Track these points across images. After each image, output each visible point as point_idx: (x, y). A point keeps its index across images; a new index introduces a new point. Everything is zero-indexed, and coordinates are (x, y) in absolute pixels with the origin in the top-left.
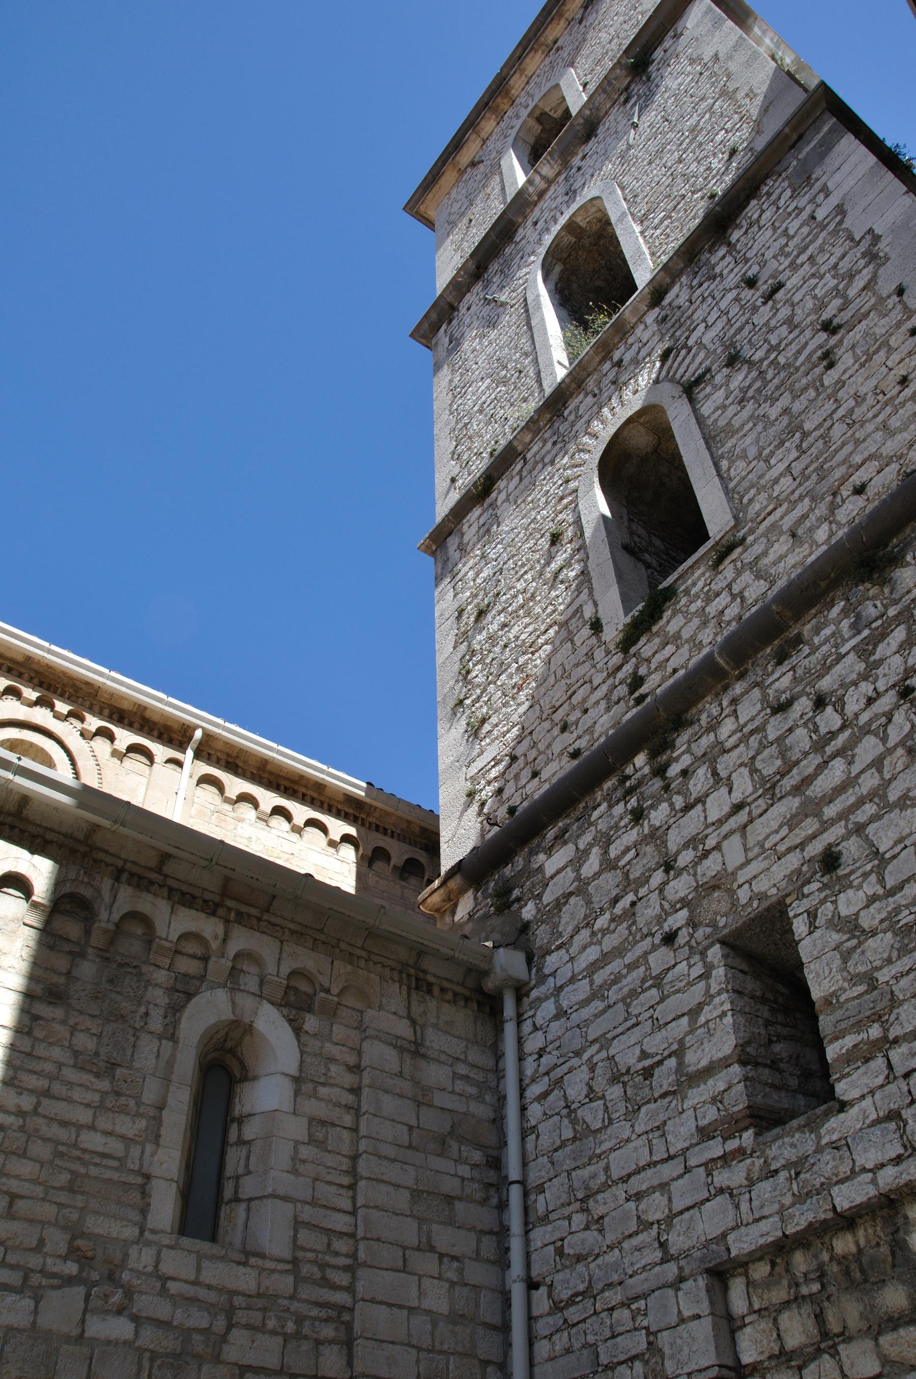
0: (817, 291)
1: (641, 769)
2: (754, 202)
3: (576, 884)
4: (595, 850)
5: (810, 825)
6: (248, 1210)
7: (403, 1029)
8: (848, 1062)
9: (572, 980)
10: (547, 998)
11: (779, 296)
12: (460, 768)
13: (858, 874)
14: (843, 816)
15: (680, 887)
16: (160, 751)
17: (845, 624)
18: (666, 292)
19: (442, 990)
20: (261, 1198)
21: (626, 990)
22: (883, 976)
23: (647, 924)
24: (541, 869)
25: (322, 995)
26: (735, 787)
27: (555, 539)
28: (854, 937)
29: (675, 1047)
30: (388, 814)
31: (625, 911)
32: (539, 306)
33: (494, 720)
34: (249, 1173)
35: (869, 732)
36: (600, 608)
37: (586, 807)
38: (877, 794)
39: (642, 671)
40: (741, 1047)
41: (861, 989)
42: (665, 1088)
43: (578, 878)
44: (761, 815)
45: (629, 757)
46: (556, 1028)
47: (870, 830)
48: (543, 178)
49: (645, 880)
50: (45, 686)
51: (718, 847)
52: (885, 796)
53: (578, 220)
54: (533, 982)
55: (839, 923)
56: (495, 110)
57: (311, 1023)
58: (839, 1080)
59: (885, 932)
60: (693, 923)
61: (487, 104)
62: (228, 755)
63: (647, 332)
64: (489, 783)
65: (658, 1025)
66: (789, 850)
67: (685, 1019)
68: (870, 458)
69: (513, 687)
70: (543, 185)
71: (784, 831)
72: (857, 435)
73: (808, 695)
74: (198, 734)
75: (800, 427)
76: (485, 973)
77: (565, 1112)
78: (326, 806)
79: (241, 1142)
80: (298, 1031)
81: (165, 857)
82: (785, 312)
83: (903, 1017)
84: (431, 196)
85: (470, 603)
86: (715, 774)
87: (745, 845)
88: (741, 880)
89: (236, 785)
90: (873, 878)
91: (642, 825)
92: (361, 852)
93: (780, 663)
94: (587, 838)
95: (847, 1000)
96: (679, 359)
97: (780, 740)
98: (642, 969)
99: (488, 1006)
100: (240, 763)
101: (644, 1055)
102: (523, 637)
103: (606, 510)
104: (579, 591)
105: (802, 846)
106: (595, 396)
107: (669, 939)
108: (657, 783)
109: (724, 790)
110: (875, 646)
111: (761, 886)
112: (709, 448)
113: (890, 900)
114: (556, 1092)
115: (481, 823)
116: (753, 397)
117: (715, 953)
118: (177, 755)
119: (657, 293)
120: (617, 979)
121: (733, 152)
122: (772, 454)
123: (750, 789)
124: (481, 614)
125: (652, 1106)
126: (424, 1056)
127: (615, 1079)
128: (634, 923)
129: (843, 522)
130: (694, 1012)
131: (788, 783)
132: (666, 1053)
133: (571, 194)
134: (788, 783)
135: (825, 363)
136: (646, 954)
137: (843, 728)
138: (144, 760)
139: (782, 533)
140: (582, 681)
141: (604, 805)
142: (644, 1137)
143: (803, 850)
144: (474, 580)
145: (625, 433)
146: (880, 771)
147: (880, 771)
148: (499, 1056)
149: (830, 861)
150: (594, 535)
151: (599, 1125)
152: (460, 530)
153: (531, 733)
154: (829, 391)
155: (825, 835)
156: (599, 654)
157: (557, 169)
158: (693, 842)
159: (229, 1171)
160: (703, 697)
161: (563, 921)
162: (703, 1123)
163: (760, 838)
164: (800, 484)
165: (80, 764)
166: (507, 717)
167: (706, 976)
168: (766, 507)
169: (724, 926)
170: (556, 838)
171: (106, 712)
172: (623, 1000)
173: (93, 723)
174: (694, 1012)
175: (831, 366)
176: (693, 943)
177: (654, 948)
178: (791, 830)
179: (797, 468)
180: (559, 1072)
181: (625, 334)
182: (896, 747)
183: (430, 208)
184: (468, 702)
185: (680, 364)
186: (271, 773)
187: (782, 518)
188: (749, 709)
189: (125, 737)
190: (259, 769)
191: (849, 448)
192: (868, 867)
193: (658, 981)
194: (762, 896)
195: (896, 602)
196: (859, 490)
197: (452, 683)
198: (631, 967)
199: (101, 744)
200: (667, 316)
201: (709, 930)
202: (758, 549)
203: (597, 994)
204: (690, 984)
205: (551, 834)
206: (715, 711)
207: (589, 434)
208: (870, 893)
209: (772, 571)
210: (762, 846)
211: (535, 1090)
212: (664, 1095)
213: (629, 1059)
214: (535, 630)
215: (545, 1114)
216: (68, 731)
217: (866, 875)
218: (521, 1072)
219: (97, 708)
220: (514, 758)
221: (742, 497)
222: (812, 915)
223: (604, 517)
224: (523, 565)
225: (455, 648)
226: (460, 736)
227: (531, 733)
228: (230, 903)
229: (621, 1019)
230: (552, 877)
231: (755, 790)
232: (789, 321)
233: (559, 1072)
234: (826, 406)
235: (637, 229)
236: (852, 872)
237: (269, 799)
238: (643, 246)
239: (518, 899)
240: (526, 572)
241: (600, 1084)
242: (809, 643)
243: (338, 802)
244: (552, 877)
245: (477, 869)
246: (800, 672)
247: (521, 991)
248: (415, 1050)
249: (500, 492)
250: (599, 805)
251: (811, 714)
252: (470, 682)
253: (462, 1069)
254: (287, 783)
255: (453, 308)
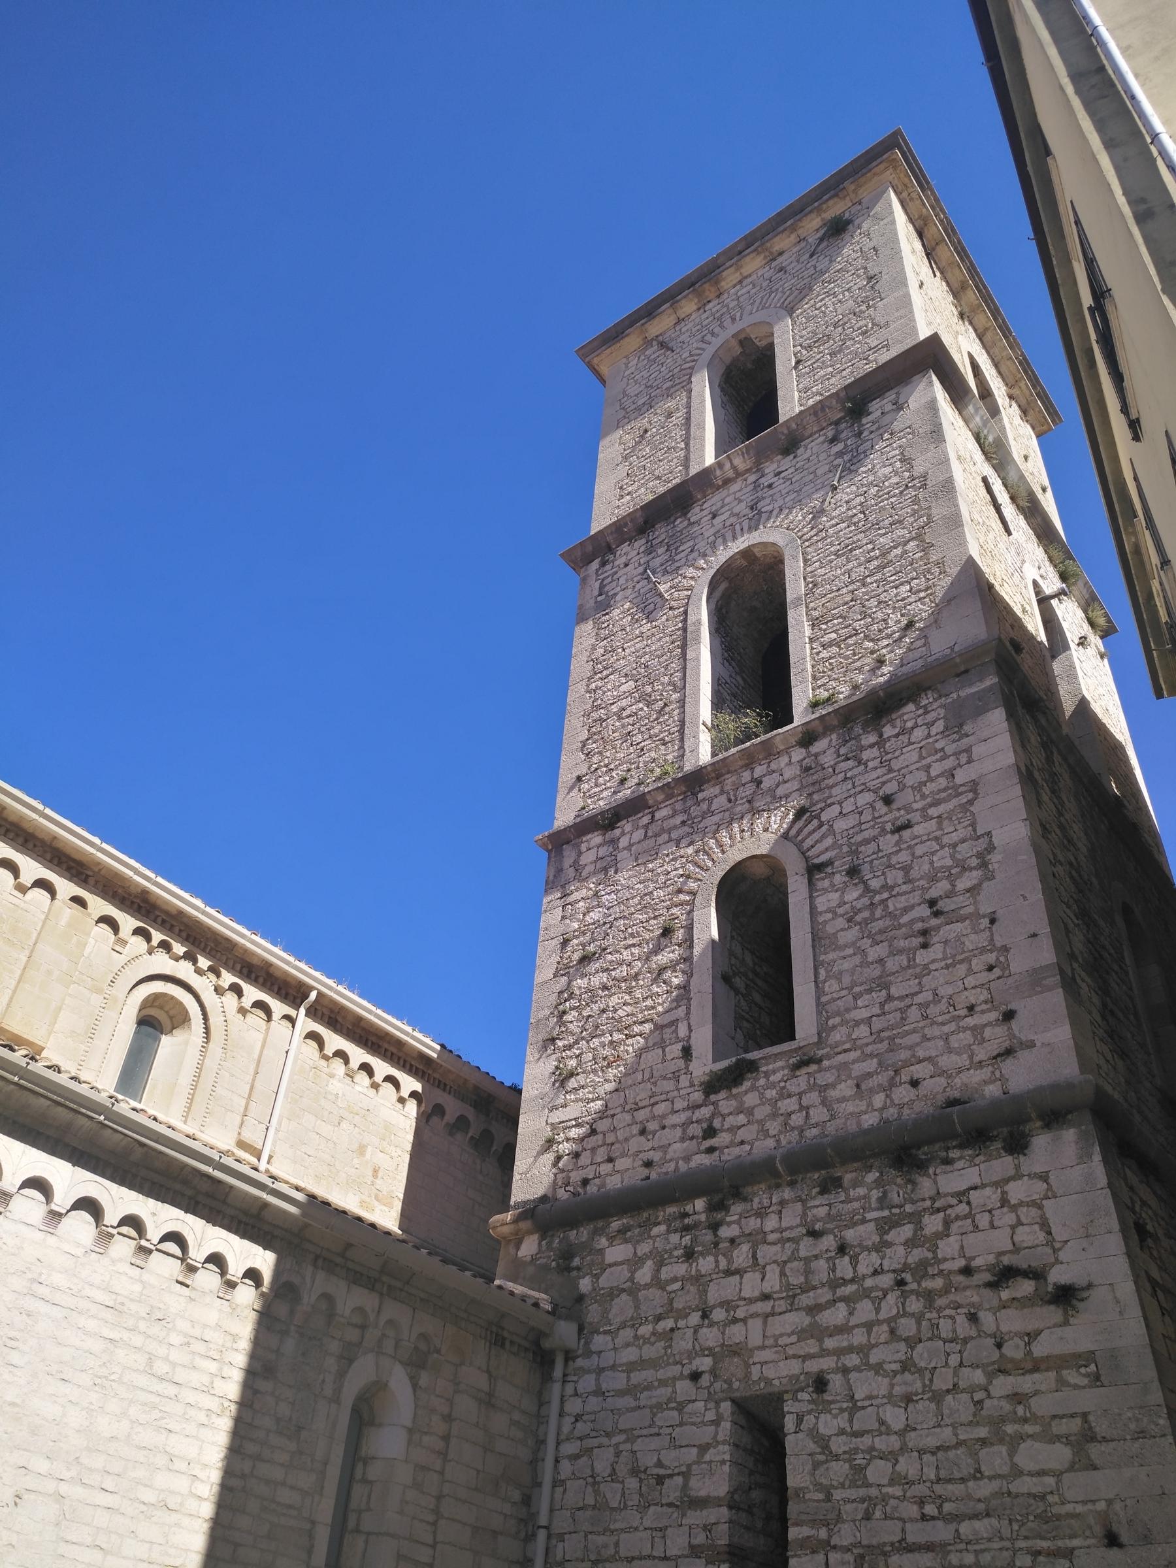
0: (935, 858)
1: (699, 1213)
2: (911, 707)
3: (629, 1284)
4: (649, 1263)
5: (811, 1347)
6: (366, 1542)
7: (483, 1382)
8: (802, 1547)
9: (613, 1367)
10: (589, 1372)
11: (906, 834)
12: (543, 1108)
13: (837, 1406)
14: (839, 1352)
15: (711, 1337)
16: (278, 1008)
17: (875, 1194)
18: (815, 740)
19: (512, 1342)
20: (378, 1534)
21: (654, 1401)
22: (837, 1495)
23: (680, 1353)
24: (601, 1251)
25: (435, 1355)
26: (767, 1278)
27: (667, 932)
28: (823, 1453)
29: (684, 1469)
30: (450, 1071)
31: (664, 1332)
32: (698, 641)
33: (581, 1079)
34: (369, 1509)
35: (868, 1297)
36: (693, 1034)
37: (648, 1219)
38: (863, 1350)
39: (717, 1124)
40: (731, 1493)
41: (821, 1496)
42: (671, 1499)
43: (631, 1279)
44: (780, 1314)
45: (692, 1195)
46: (594, 1403)
47: (853, 1376)
48: (734, 467)
49: (683, 1314)
50: (191, 940)
51: (744, 1321)
52: (867, 1356)
53: (756, 550)
54: (580, 1352)
55: (814, 1434)
56: (699, 295)
57: (424, 1379)
58: (793, 1556)
59: (845, 1461)
60: (713, 1372)
61: (693, 284)
62: (332, 1011)
63: (789, 764)
64: (568, 1140)
65: (674, 1444)
66: (795, 1356)
67: (695, 1451)
68: (929, 1059)
69: (604, 1059)
70: (731, 474)
71: (794, 1338)
72: (926, 1031)
73: (836, 1236)
74: (313, 995)
75: (887, 987)
76: (546, 1335)
77: (590, 1480)
78: (402, 1062)
79: (365, 1481)
80: (415, 1386)
81: (349, 1246)
82: (904, 857)
83: (843, 1532)
84: (608, 351)
85: (577, 937)
86: (754, 1256)
87: (764, 1331)
88: (756, 1360)
89: (335, 1041)
90: (846, 1414)
91: (691, 1265)
92: (422, 1109)
93: (822, 1193)
94: (644, 1248)
95: (810, 1500)
96: (810, 827)
97: (807, 1260)
98: (670, 1389)
99: (542, 1358)
100: (339, 1019)
101: (659, 1464)
102: (621, 1013)
103: (715, 934)
104: (677, 1000)
105: (805, 1358)
106: (730, 801)
107: (695, 1376)
108: (708, 1237)
109: (758, 1275)
110: (890, 1229)
111: (770, 1372)
112: (814, 947)
113: (854, 1440)
114: (585, 1459)
115: (555, 1175)
116: (860, 924)
117: (726, 1407)
118: (292, 1012)
119: (808, 738)
120: (649, 1387)
121: (910, 624)
122: (860, 995)
123: (777, 1288)
124: (585, 959)
125: (658, 1508)
126: (493, 1406)
127: (635, 1472)
128: (670, 1346)
129: (896, 1102)
130: (703, 1448)
131: (806, 1300)
132: (676, 1471)
133: (756, 517)
134: (806, 1300)
135: (921, 940)
136: (675, 1379)
137: (852, 1281)
138: (263, 1015)
139: (850, 1077)
140: (664, 1097)
141: (663, 1228)
142: (649, 1532)
143: (804, 1362)
144: (584, 915)
145: (748, 863)
146: (869, 1333)
147: (869, 1333)
148: (541, 1404)
149: (820, 1384)
150: (703, 954)
151: (616, 1505)
152: (578, 846)
153: (613, 1116)
154: (918, 970)
155: (821, 1360)
156: (684, 1081)
157: (749, 464)
158: (727, 1305)
159: (353, 1505)
160: (759, 1183)
161: (614, 1311)
162: (695, 1542)
163: (777, 1333)
164: (874, 1042)
165: (211, 1021)
166: (594, 1085)
167: (716, 1423)
168: (844, 1043)
169: (737, 1390)
170: (619, 1231)
171: (238, 967)
172: (651, 1407)
173: (228, 978)
174: (703, 1448)
175: (925, 946)
176: (712, 1390)
177: (681, 1377)
178: (799, 1341)
179: (877, 1024)
180: (589, 1443)
181: (770, 755)
182: (884, 1321)
183: (606, 362)
184: (560, 1043)
185: (810, 833)
186: (363, 1029)
187: (854, 1062)
188: (791, 1217)
189: (252, 993)
190: (354, 1025)
191: (916, 1038)
192: (845, 1405)
193: (680, 1407)
194: (768, 1382)
195: (914, 1202)
196: (915, 1083)
197: (547, 1012)
198: (663, 1383)
199: (230, 999)
200: (810, 768)
201: (725, 1386)
202: (829, 1077)
203: (630, 1391)
204: (703, 1423)
205: (616, 1225)
206: (766, 1202)
207: (716, 839)
208: (842, 1426)
209: (835, 1106)
210: (776, 1340)
211: (569, 1448)
212: (670, 1505)
213: (649, 1460)
214: (633, 1014)
215: (573, 1474)
216: (204, 985)
217: (842, 1410)
218: (559, 1427)
219: (231, 963)
220: (593, 1132)
221: (828, 1018)
222: (800, 1419)
223: (713, 941)
224: (632, 935)
225: (555, 976)
226: (547, 1074)
227: (613, 1116)
228: (385, 1279)
229: (647, 1424)
230: (610, 1266)
231: (780, 1291)
232: (906, 869)
233: (589, 1443)
234: (911, 983)
235: (808, 632)
236: (833, 1402)
237: (358, 1055)
238: (808, 659)
239: (578, 1269)
240: (634, 945)
241: (622, 1470)
242: (846, 1191)
243: (413, 1058)
244: (610, 1266)
245: (544, 1216)
246: (834, 1211)
247: (569, 1356)
248: (488, 1401)
249: (623, 834)
250: (659, 1224)
251: (833, 1254)
252: (564, 1024)
253: (516, 1416)
254: (374, 1039)
255: (610, 549)
